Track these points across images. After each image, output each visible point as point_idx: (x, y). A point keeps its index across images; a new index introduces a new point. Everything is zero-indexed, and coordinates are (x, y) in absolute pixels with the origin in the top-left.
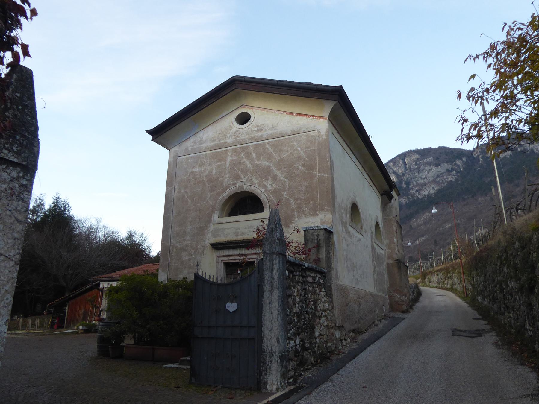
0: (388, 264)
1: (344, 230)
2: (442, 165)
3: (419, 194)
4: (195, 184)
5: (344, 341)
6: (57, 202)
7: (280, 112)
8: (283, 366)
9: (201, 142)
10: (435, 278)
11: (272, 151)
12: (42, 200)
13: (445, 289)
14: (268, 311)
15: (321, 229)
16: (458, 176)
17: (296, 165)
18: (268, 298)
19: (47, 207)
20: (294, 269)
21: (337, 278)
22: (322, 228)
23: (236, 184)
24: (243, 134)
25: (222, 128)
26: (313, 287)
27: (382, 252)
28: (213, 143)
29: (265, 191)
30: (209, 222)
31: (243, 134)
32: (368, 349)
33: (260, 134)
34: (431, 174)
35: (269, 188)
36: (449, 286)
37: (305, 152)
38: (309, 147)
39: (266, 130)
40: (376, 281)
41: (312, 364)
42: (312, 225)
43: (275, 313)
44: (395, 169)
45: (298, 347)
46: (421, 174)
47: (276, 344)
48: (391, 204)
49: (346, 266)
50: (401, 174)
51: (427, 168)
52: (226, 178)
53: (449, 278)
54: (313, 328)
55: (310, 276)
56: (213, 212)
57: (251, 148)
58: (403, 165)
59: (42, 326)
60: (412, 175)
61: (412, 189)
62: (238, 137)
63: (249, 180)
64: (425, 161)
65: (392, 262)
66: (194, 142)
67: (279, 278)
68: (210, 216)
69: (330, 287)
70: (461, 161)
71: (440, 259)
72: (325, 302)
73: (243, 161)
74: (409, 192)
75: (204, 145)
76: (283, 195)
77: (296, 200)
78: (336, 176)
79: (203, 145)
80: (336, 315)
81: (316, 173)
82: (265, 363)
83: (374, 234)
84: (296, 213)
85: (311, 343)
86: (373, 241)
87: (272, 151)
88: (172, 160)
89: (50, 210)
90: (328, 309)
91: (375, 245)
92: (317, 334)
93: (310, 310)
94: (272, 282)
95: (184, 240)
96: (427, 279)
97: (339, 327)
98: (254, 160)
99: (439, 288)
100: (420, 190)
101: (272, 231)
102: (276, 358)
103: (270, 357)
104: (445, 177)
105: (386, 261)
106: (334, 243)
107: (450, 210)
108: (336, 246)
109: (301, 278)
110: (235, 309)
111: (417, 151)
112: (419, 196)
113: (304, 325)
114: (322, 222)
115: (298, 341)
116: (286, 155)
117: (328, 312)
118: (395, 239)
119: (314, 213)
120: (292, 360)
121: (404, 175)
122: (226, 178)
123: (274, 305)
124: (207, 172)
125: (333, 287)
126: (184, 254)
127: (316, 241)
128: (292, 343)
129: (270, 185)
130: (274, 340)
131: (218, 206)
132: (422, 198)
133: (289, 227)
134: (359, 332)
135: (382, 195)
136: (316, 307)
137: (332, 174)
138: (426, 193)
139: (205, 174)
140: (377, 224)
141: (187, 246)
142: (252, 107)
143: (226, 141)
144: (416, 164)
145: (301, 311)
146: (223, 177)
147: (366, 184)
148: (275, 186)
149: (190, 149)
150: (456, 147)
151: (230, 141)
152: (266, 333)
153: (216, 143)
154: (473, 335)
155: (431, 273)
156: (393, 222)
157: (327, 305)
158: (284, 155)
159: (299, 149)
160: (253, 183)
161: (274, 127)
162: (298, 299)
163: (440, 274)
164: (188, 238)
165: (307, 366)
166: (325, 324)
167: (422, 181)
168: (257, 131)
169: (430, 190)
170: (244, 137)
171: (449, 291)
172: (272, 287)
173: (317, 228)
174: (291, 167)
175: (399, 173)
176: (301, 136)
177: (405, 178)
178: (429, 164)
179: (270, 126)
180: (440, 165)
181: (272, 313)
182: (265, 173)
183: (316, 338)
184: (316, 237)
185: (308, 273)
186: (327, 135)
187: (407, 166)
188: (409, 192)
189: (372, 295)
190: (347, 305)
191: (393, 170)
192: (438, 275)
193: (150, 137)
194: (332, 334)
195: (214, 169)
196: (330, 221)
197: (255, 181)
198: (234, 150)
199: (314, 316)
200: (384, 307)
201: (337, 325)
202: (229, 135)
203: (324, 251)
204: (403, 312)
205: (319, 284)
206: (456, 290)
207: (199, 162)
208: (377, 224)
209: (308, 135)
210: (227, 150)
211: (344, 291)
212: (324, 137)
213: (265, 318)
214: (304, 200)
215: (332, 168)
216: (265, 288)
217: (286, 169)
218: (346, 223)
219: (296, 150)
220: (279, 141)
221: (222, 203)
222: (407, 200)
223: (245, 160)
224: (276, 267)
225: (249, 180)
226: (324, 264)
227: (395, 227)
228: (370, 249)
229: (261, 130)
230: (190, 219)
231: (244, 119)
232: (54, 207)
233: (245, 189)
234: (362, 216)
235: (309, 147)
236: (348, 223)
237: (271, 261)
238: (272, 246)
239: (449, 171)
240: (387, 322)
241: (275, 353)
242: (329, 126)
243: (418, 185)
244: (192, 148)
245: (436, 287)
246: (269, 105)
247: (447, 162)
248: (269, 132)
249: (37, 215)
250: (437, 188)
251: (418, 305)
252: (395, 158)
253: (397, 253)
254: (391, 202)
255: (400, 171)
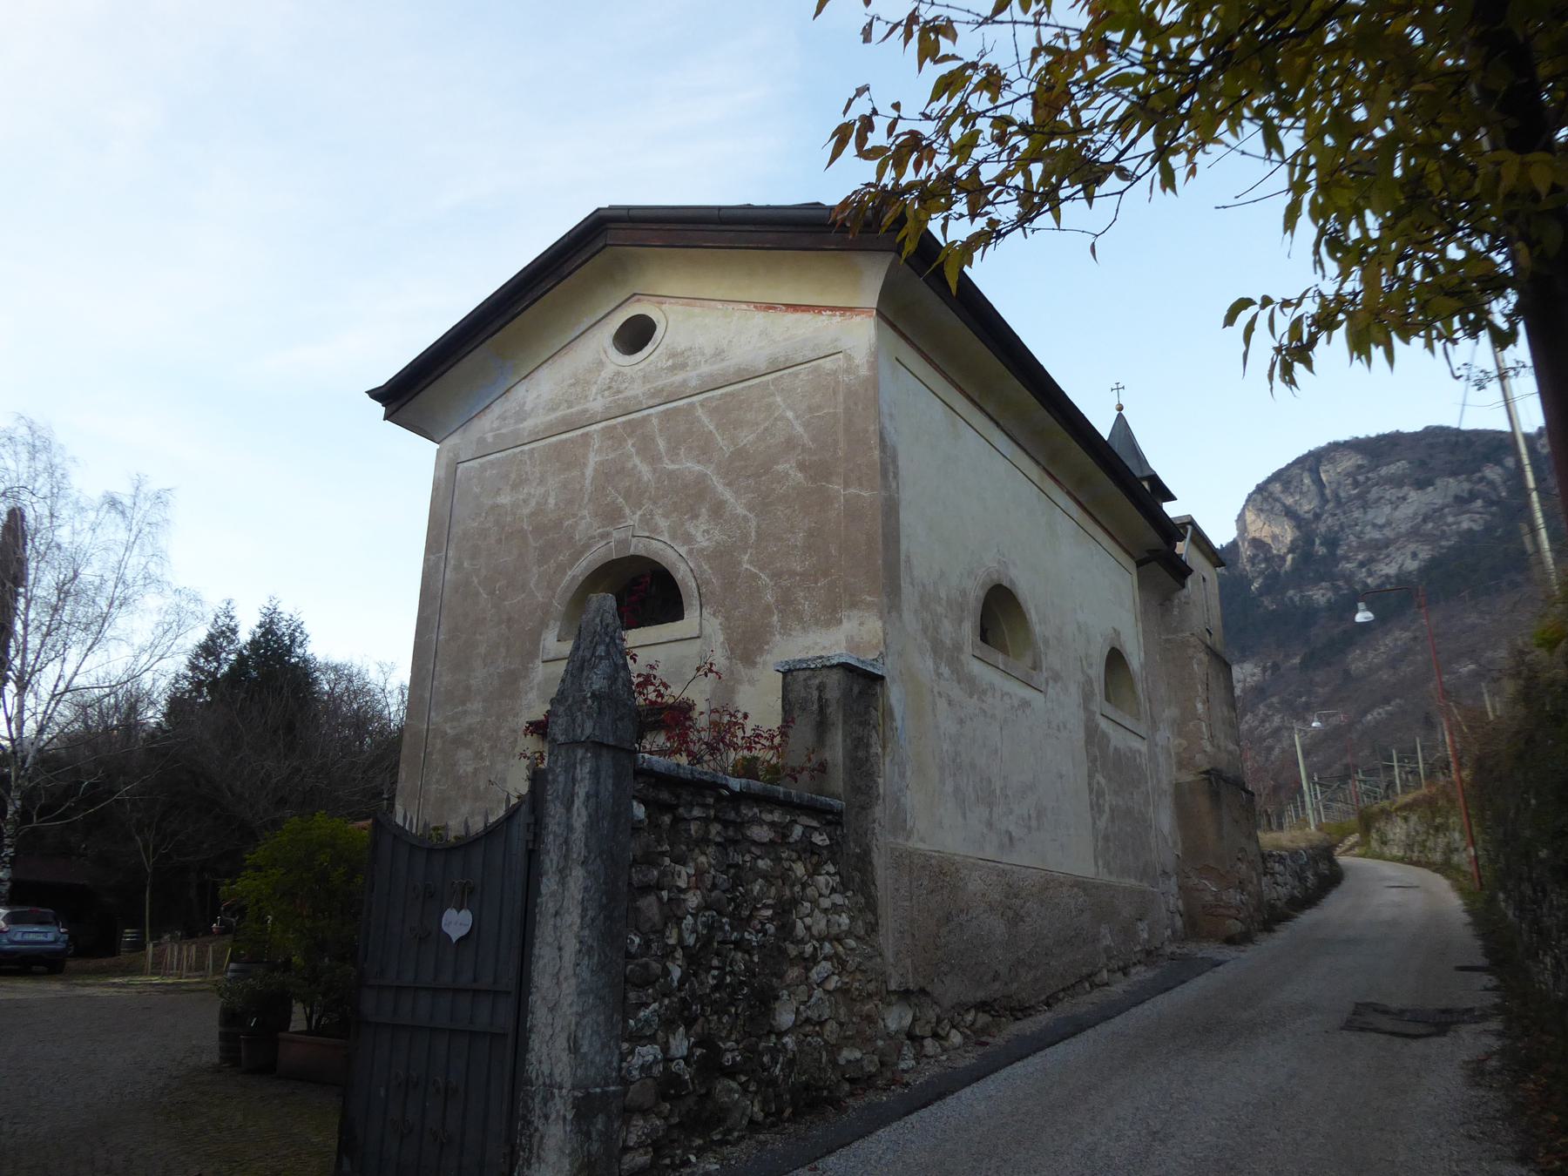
0: (1178, 787)
1: (945, 671)
2: (1439, 482)
3: (1370, 574)
4: (499, 541)
5: (928, 1042)
6: (272, 621)
7: (736, 306)
8: (588, 1135)
9: (521, 416)
10: (1398, 831)
11: (712, 428)
12: (232, 618)
13: (1428, 865)
14: (550, 940)
15: (832, 667)
16: (1493, 515)
17: (780, 467)
18: (553, 894)
19: (244, 637)
20: (678, 797)
21: (900, 825)
22: (834, 662)
23: (608, 534)
24: (633, 380)
25: (583, 369)
26: (778, 860)
27: (1137, 744)
28: (553, 416)
29: (690, 552)
30: (532, 655)
31: (633, 380)
32: (1004, 1073)
33: (679, 377)
34: (1406, 511)
35: (702, 542)
36: (1438, 857)
37: (806, 425)
38: (819, 407)
39: (697, 365)
40: (1106, 838)
41: (751, 1121)
42: (802, 656)
43: (571, 946)
44: (1289, 501)
45: (679, 1066)
46: (1371, 514)
47: (565, 1057)
48: (1185, 592)
49: (949, 788)
50: (1310, 516)
51: (1391, 493)
52: (583, 518)
53: (1437, 829)
54: (765, 1000)
55: (761, 822)
56: (544, 624)
57: (655, 421)
58: (1313, 488)
59: (200, 967)
60: (1343, 518)
61: (1347, 559)
62: (619, 392)
63: (646, 521)
64: (1384, 471)
65: (1190, 778)
66: (503, 418)
67: (592, 824)
68: (535, 637)
69: (864, 861)
70: (1499, 470)
71: (1414, 772)
72: (836, 909)
73: (630, 465)
74: (1336, 570)
75: (529, 424)
76: (740, 563)
77: (777, 575)
78: (906, 495)
79: (525, 424)
80: (889, 954)
81: (836, 487)
82: (530, 1123)
83: (1099, 688)
84: (775, 618)
85: (752, 1052)
86: (1095, 708)
87: (712, 428)
88: (442, 473)
89: (254, 643)
90: (849, 933)
91: (1104, 724)
92: (785, 1017)
93: (752, 938)
94: (566, 841)
95: (465, 712)
96: (1374, 835)
97: (905, 995)
98: (660, 459)
99: (1412, 863)
100: (1371, 560)
101: (581, 669)
102: (561, 1106)
103: (545, 1101)
104: (1450, 519)
105: (1166, 775)
106: (889, 713)
107: (1473, 618)
108: (898, 723)
109: (715, 828)
110: (464, 931)
111: (1356, 445)
112: (1369, 581)
113: (716, 988)
114: (853, 645)
115: (680, 1044)
116: (751, 437)
117: (852, 943)
118: (1199, 706)
119: (830, 615)
120: (644, 1112)
121: (1317, 516)
122: (583, 518)
123: (568, 919)
124: (533, 503)
125: (879, 860)
126: (463, 754)
127: (816, 706)
128: (649, 1052)
129: (704, 533)
130: (561, 1042)
131: (558, 606)
132: (1378, 586)
133: (753, 664)
134: (1012, 1009)
135: (1140, 564)
136: (786, 930)
137: (886, 487)
138: (1392, 570)
139: (526, 511)
140: (1115, 659)
141: (471, 730)
142: (661, 298)
143: (588, 405)
144: (1356, 484)
145: (705, 942)
146: (574, 515)
147: (1065, 526)
148: (717, 535)
149: (489, 437)
150: (1481, 427)
151: (596, 405)
152: (540, 1016)
153: (559, 414)
154: (1412, 1028)
155: (1386, 814)
156: (1190, 651)
157: (844, 920)
158: (746, 437)
159: (790, 414)
160: (655, 529)
161: (719, 354)
162: (693, 900)
163: (1414, 818)
164: (476, 705)
165: (729, 1131)
166: (832, 984)
167: (1377, 535)
168: (673, 368)
169: (1404, 561)
170: (637, 390)
171: (1436, 871)
172: (566, 857)
173: (819, 663)
174: (766, 473)
175: (1301, 512)
176: (796, 375)
177: (1322, 528)
178: (1397, 482)
179: (709, 351)
180: (1430, 483)
181: (560, 949)
182: (691, 498)
183: (780, 1035)
184: (815, 694)
185: (748, 812)
186: (874, 366)
187: (1327, 491)
188: (1336, 570)
189: (1080, 884)
190: (948, 918)
191: (1284, 505)
192: (1406, 819)
193: (379, 409)
194: (869, 1019)
195: (553, 494)
196: (875, 642)
197: (663, 523)
198: (609, 433)
199: (775, 956)
200: (1141, 925)
201: (893, 986)
202: (594, 389)
203: (839, 738)
204: (1230, 941)
205: (807, 849)
206: (1457, 868)
207: (513, 476)
208: (1115, 659)
209: (816, 369)
210: (587, 434)
211: (940, 874)
212: (864, 371)
213: (541, 963)
214: (801, 575)
215: (888, 467)
216: (548, 861)
217: (751, 481)
218: (958, 648)
219: (782, 418)
220: (732, 394)
221: (569, 595)
222: (1330, 594)
223: (637, 460)
224: (581, 791)
225: (646, 521)
226: (838, 780)
227: (1199, 665)
228: (1080, 735)
229: (684, 366)
230: (482, 650)
231: (636, 335)
232: (263, 635)
233: (632, 551)
234: (1037, 628)
235: (819, 407)
236: (968, 649)
237: (570, 768)
238: (574, 721)
239: (1461, 501)
240: (1150, 974)
241: (561, 1088)
242: (879, 337)
243: (1363, 546)
244: (496, 436)
245: (1401, 860)
246: (711, 286)
247: (1454, 474)
248: (705, 369)
249: (217, 659)
250: (1425, 553)
251: (1307, 917)
252: (1289, 466)
253: (1209, 748)
254: (1183, 586)
255: (1306, 508)
